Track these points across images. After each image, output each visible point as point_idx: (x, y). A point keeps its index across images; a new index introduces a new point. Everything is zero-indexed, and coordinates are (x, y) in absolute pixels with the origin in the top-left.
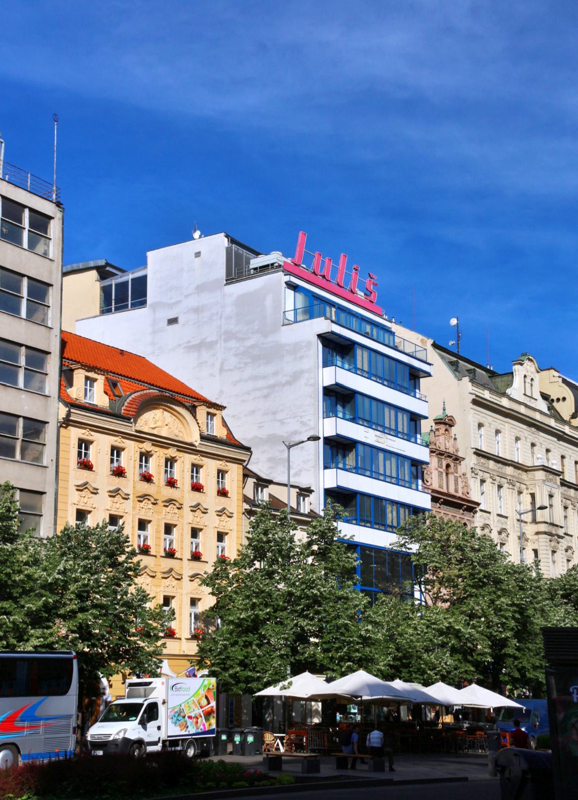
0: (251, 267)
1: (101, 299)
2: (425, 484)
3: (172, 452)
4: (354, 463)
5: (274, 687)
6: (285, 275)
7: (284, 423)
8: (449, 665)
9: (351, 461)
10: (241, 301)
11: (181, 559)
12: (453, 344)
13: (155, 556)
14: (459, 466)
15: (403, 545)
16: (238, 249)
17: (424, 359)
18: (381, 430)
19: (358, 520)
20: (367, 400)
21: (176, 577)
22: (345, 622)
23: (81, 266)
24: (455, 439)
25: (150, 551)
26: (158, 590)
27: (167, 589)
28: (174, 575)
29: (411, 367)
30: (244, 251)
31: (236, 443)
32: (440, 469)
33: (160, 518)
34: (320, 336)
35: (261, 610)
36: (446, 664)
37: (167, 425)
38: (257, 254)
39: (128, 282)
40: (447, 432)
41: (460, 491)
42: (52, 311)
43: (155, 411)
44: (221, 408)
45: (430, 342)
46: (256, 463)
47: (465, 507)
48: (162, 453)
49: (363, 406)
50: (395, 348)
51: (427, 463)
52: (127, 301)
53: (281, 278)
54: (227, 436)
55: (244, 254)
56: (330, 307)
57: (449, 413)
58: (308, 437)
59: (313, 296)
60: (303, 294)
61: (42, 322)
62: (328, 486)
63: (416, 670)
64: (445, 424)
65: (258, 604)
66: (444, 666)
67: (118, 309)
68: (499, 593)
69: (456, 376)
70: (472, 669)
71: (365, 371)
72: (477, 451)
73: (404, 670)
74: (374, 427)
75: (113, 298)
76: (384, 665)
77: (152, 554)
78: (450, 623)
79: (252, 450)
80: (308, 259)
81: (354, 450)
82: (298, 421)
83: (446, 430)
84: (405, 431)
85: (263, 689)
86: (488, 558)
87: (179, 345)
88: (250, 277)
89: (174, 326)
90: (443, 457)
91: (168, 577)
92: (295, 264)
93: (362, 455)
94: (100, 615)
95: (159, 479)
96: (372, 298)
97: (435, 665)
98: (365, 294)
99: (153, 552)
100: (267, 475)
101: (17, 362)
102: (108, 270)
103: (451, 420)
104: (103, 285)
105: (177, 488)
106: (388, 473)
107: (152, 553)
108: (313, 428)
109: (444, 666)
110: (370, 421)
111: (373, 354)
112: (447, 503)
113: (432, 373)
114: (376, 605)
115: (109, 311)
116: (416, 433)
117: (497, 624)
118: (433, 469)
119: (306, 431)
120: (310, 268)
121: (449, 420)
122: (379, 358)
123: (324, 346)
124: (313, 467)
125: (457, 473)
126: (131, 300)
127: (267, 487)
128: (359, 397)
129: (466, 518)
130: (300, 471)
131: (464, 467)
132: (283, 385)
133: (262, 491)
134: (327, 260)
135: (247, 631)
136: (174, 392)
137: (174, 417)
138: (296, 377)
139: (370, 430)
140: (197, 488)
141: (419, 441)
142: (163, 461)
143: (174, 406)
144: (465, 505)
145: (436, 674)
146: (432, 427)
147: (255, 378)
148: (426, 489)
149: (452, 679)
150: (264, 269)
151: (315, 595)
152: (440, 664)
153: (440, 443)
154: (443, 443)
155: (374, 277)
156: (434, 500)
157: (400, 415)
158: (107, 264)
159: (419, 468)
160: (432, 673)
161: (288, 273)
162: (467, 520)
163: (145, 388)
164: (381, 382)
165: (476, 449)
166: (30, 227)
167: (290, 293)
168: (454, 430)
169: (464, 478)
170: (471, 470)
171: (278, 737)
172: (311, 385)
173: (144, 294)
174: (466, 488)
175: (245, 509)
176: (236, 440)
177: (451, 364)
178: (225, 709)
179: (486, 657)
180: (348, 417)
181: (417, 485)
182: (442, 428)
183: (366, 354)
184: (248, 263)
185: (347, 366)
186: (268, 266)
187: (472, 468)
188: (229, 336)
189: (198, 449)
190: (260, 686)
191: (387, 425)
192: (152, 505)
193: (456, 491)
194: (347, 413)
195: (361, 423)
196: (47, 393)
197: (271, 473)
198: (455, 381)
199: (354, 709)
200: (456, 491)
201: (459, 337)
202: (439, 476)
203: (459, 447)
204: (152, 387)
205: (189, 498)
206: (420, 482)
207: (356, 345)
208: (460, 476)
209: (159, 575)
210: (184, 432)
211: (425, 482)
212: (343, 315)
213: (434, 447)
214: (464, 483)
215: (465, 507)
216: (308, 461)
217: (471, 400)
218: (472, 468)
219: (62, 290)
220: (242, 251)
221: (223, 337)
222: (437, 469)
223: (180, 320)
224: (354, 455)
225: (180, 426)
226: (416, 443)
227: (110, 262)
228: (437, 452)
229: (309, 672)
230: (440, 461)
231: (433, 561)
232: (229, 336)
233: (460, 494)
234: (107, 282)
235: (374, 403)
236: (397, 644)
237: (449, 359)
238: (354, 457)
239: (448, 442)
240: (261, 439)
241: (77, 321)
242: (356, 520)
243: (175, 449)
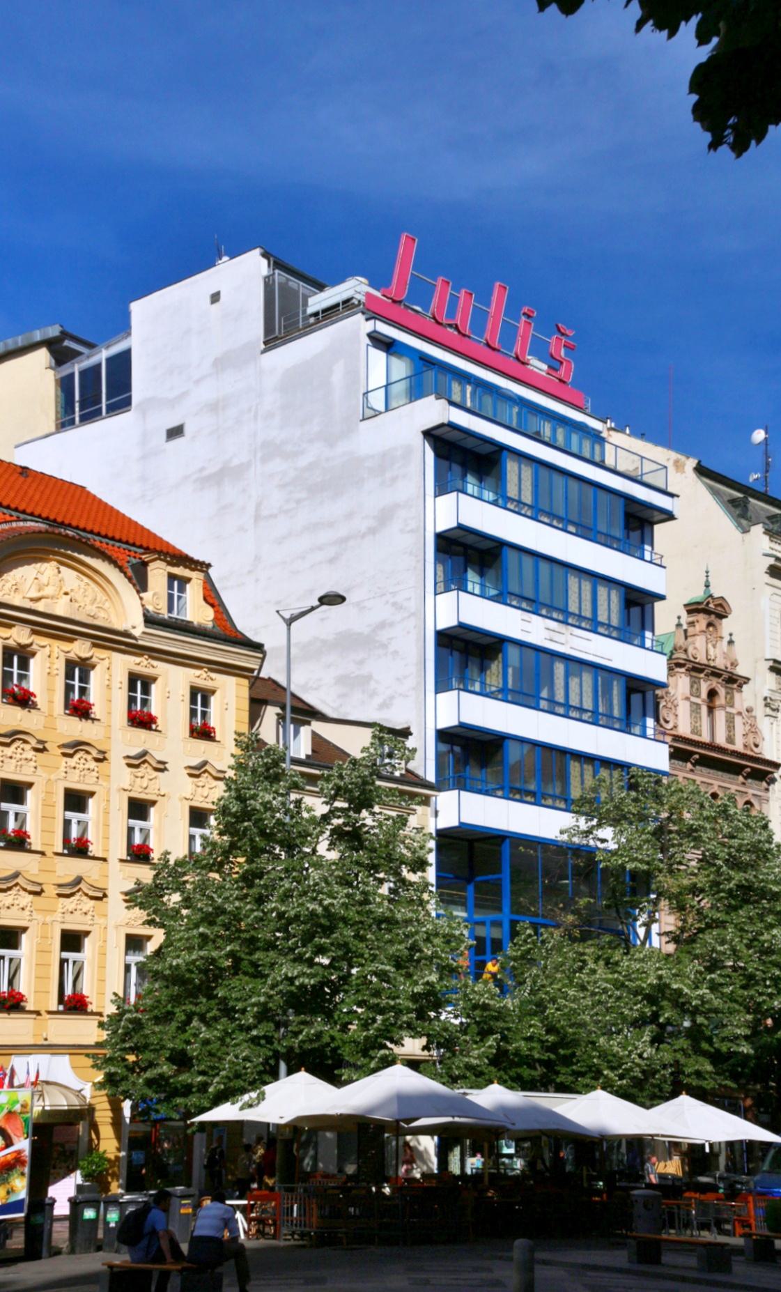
0: (310, 310)
1: (57, 402)
2: (661, 726)
3: (80, 649)
4: (501, 681)
5: (233, 1104)
6: (367, 320)
7: (364, 607)
8: (647, 1059)
9: (494, 678)
10: (293, 381)
11: (104, 860)
12: (757, 479)
13: (43, 853)
14: (737, 695)
15: (588, 832)
16: (288, 280)
17: (662, 486)
18: (561, 618)
19: (507, 789)
20: (528, 561)
21: (91, 893)
22: (381, 967)
23: (20, 341)
24: (731, 642)
25: (30, 844)
26: (48, 919)
27: (68, 917)
28: (87, 891)
29: (629, 500)
30: (301, 283)
32: (694, 699)
33: (53, 777)
34: (429, 435)
35: (217, 948)
36: (640, 1056)
37: (66, 594)
38: (321, 287)
39: (99, 366)
40: (711, 629)
43: (39, 565)
45: (691, 463)
46: (316, 689)
47: (749, 770)
48: (56, 650)
50: (601, 465)
51: (662, 685)
52: (100, 402)
53: (358, 326)
55: (301, 290)
56: (460, 383)
58: (322, 593)
59: (421, 359)
60: (408, 360)
62: (442, 725)
63: (583, 1070)
64: (707, 612)
65: (212, 937)
66: (637, 1060)
67: (87, 418)
68: (770, 919)
69: (739, 525)
70: (709, 1068)
71: (525, 504)
72: (777, 665)
73: (563, 1070)
74: (544, 612)
75: (77, 397)
76: (479, 1057)
77: (33, 848)
78: (660, 978)
79: (266, 648)
80: (421, 292)
81: (500, 656)
82: (387, 602)
83: (710, 625)
84: (615, 622)
85: (210, 1109)
86: (748, 851)
87: (186, 478)
88: (308, 329)
89: (178, 442)
90: (702, 675)
91: (72, 895)
92: (394, 301)
93: (517, 664)
95: (51, 702)
96: (562, 373)
97: (621, 1058)
98: (550, 367)
99: (35, 842)
100: (334, 709)
102: (67, 348)
103: (721, 605)
104: (59, 376)
105: (93, 720)
106: (574, 701)
107: (36, 846)
108: (413, 614)
109: (637, 1060)
110: (533, 601)
111: (544, 472)
112: (706, 762)
113: (676, 513)
114: (515, 945)
115: (71, 423)
116: (643, 628)
117: (764, 980)
118: (680, 698)
119: (403, 620)
120: (428, 312)
121: (716, 605)
122: (559, 480)
123: (438, 455)
124: (414, 689)
125: (732, 706)
126: (108, 399)
127: (309, 723)
128: (510, 556)
129: (751, 791)
130: (392, 698)
131: (748, 697)
132: (363, 536)
133: (297, 733)
134: (462, 295)
135: (192, 992)
136: (84, 530)
137: (86, 580)
138: (385, 517)
139: (534, 617)
140: (142, 721)
141: (648, 644)
142: (60, 667)
143: (82, 557)
144: (748, 766)
145: (621, 1077)
146: (679, 618)
147: (312, 528)
148: (661, 734)
149: (658, 1086)
150: (330, 314)
151: (313, 913)
152: (629, 1055)
153: (695, 648)
154: (700, 648)
155: (567, 332)
156: (678, 755)
157: (602, 591)
158: (65, 335)
159: (649, 695)
160: (611, 1075)
161: (372, 315)
162: (754, 795)
163: (8, 518)
164: (560, 526)
165: (775, 661)
167: (379, 356)
168: (726, 626)
169: (749, 718)
170: (763, 703)
171: (238, 1206)
172: (411, 531)
173: (127, 386)
174: (751, 736)
176: (237, 631)
177: (733, 503)
178: (204, 1150)
179: (738, 1045)
180: (493, 592)
181: (644, 727)
182: (702, 620)
183: (527, 472)
184: (305, 304)
185: (488, 495)
186: (337, 305)
187: (765, 699)
188: (270, 451)
189: (140, 642)
190: (206, 1104)
191: (573, 608)
192: (34, 753)
193: (730, 740)
194: (488, 585)
195: (514, 603)
197: (341, 705)
198: (737, 533)
199: (508, 1147)
200: (730, 740)
201: (767, 464)
202: (692, 711)
204: (22, 516)
205: (125, 741)
206: (650, 722)
207: (505, 453)
208: (740, 713)
209: (51, 891)
210: (112, 610)
211: (662, 722)
212: (488, 400)
213: (683, 656)
214: (748, 727)
215: (749, 770)
216: (405, 677)
217: (765, 567)
218: (765, 699)
220: (295, 283)
221: (259, 455)
222: (687, 699)
223: (187, 430)
224: (501, 665)
225: (100, 595)
226: (642, 646)
227: (69, 330)
228: (689, 665)
229: (307, 1071)
230: (694, 683)
231: (636, 859)
232: (270, 451)
233: (738, 746)
234: (65, 370)
235: (544, 567)
236: (547, 1018)
237: (730, 495)
238: (501, 670)
239: (714, 646)
240: (324, 642)
241: (17, 447)
242: (502, 788)
243: (88, 643)
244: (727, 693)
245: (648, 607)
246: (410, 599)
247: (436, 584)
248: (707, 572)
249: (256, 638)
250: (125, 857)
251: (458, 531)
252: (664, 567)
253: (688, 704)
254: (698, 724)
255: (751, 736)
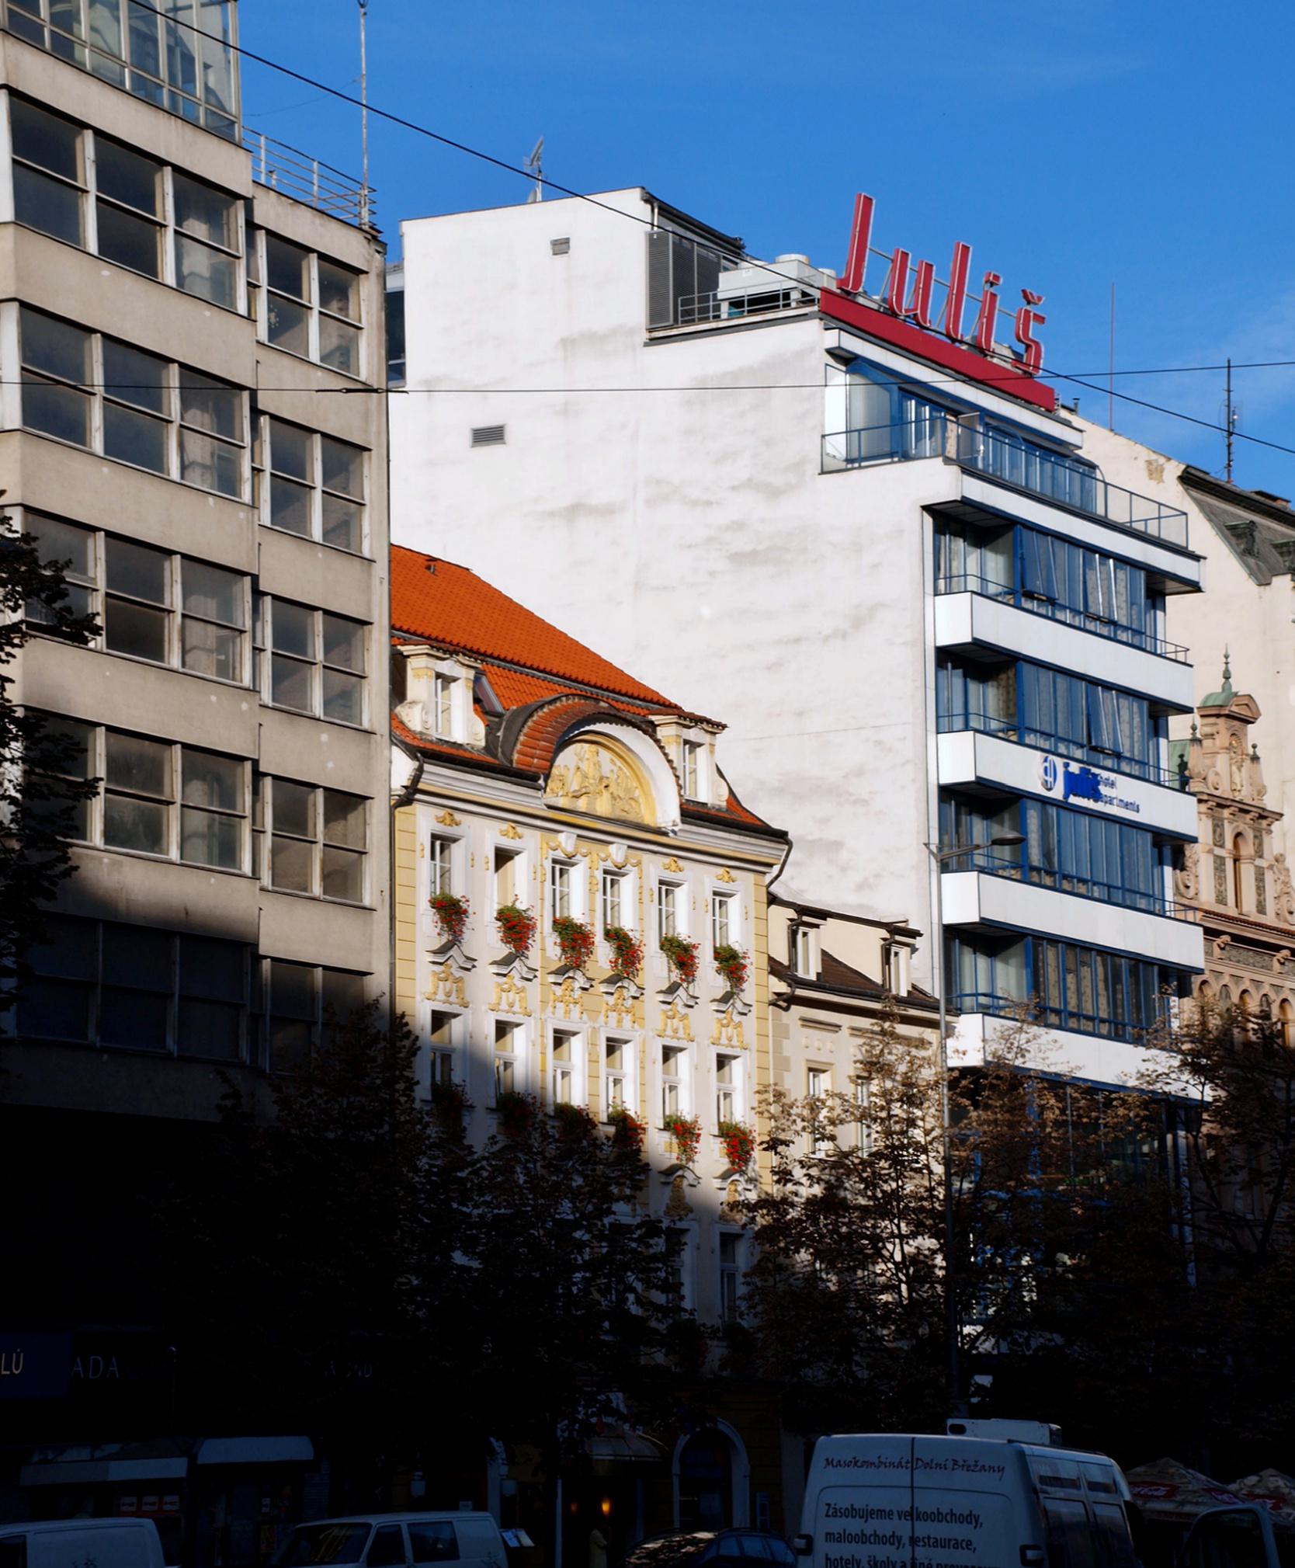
14: (1266, 838)
24: (1255, 758)
31: (749, 820)
32: (1218, 851)
33: (596, 1025)
41: (1271, 906)
42: (370, 517)
44: (715, 727)
45: (1174, 469)
49: (1038, 691)
54: (728, 801)
57: (1239, 686)
61: (347, 547)
69: (1252, 573)
79: (790, 837)
94: (871, 1164)
101: (305, 654)
122: (1063, 550)
125: (1261, 857)
128: (1027, 669)
132: (827, 639)
138: (859, 620)
143: (587, 728)
153: (1217, 774)
166: (99, 189)
167: (840, 377)
174: (1285, 898)
175: (778, 994)
193: (1261, 909)
196: (366, 725)
198: (1250, 585)
200: (1261, 909)
202: (1216, 869)
203: (1266, 783)
214: (1279, 886)
219: (388, 461)
222: (1210, 851)
233: (1270, 919)
244: (1255, 837)
245: (1162, 721)
246: (905, 738)
247: (938, 717)
248: (1226, 657)
249: (776, 825)
250: (717, 1133)
251: (974, 647)
252: (1191, 666)
253: (1211, 858)
254: (1222, 888)
255: (1285, 898)
